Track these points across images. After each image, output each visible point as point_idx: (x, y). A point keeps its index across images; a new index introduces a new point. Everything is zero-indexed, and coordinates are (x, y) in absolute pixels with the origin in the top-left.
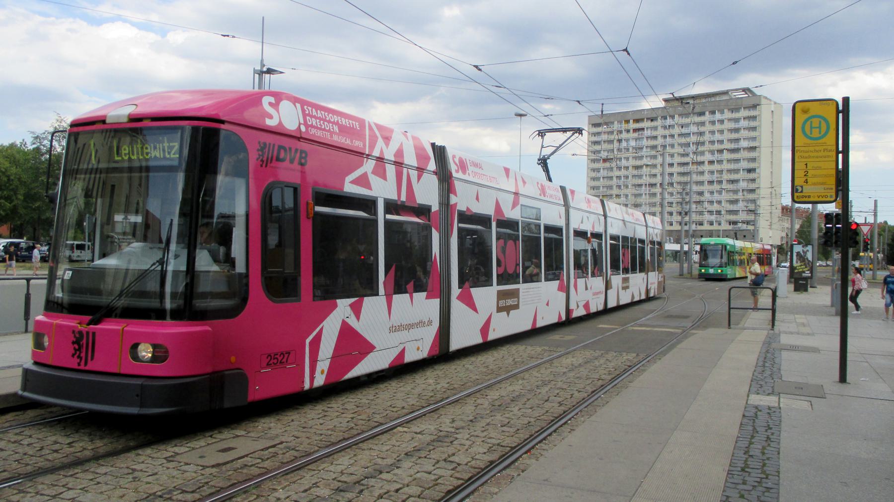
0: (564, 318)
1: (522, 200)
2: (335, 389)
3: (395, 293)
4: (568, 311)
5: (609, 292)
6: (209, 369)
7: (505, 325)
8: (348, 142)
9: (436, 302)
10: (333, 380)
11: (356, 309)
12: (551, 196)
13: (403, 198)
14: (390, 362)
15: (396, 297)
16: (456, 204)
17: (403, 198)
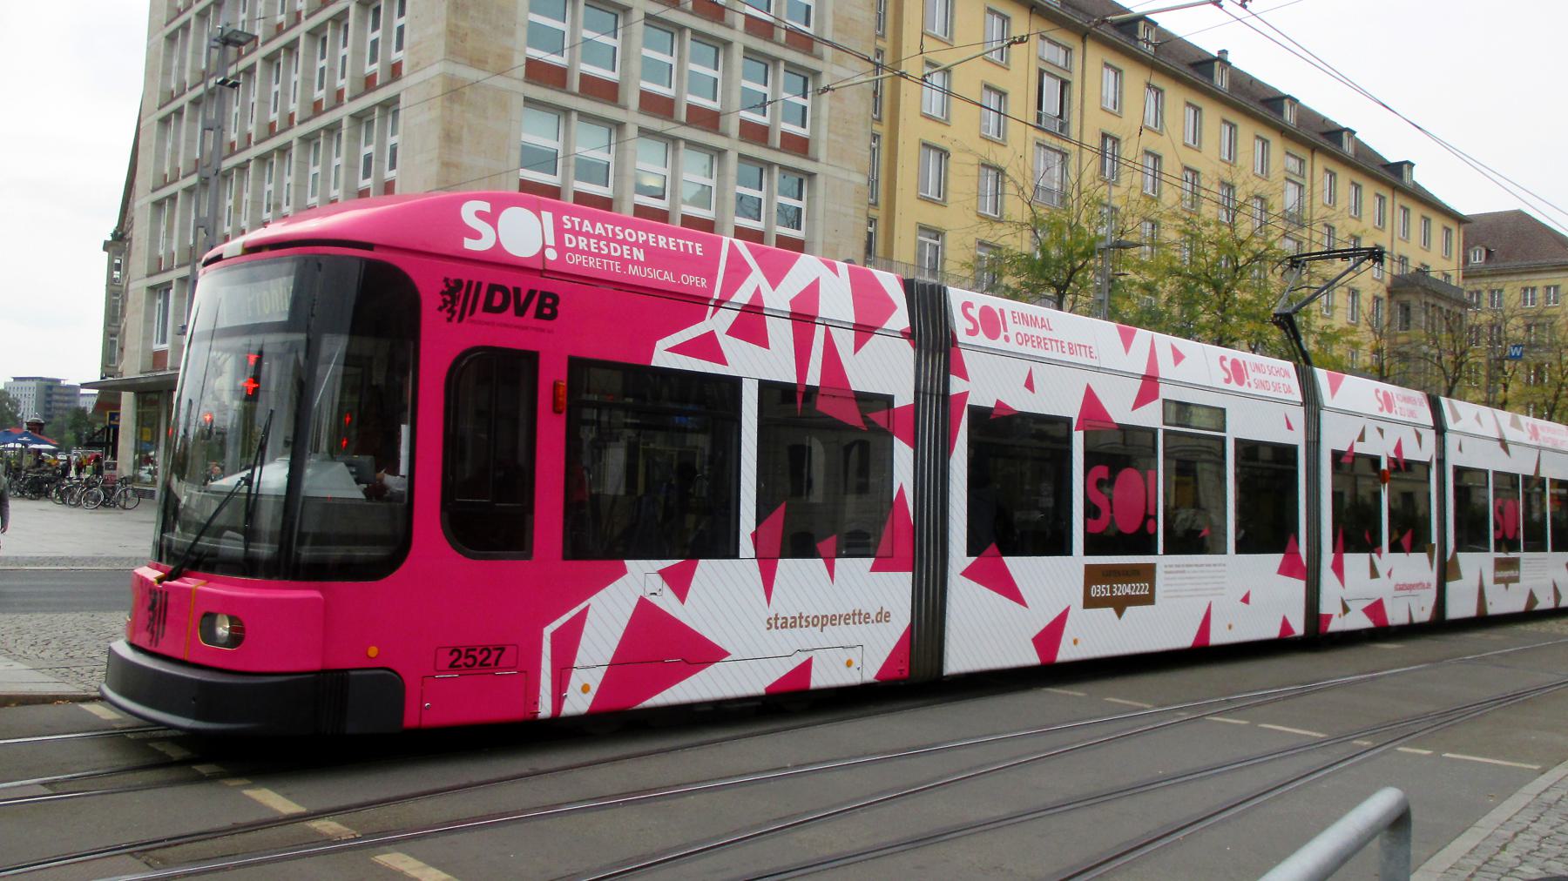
0: (1299, 629)
1: (1165, 392)
2: (619, 722)
3: (782, 557)
4: (1313, 614)
5: (1451, 586)
6: (316, 665)
7: (1095, 635)
8: (668, 277)
9: (901, 583)
10: (615, 703)
11: (679, 583)
12: (1262, 384)
13: (814, 378)
14: (768, 683)
15: (784, 565)
16: (965, 394)
17: (814, 378)
